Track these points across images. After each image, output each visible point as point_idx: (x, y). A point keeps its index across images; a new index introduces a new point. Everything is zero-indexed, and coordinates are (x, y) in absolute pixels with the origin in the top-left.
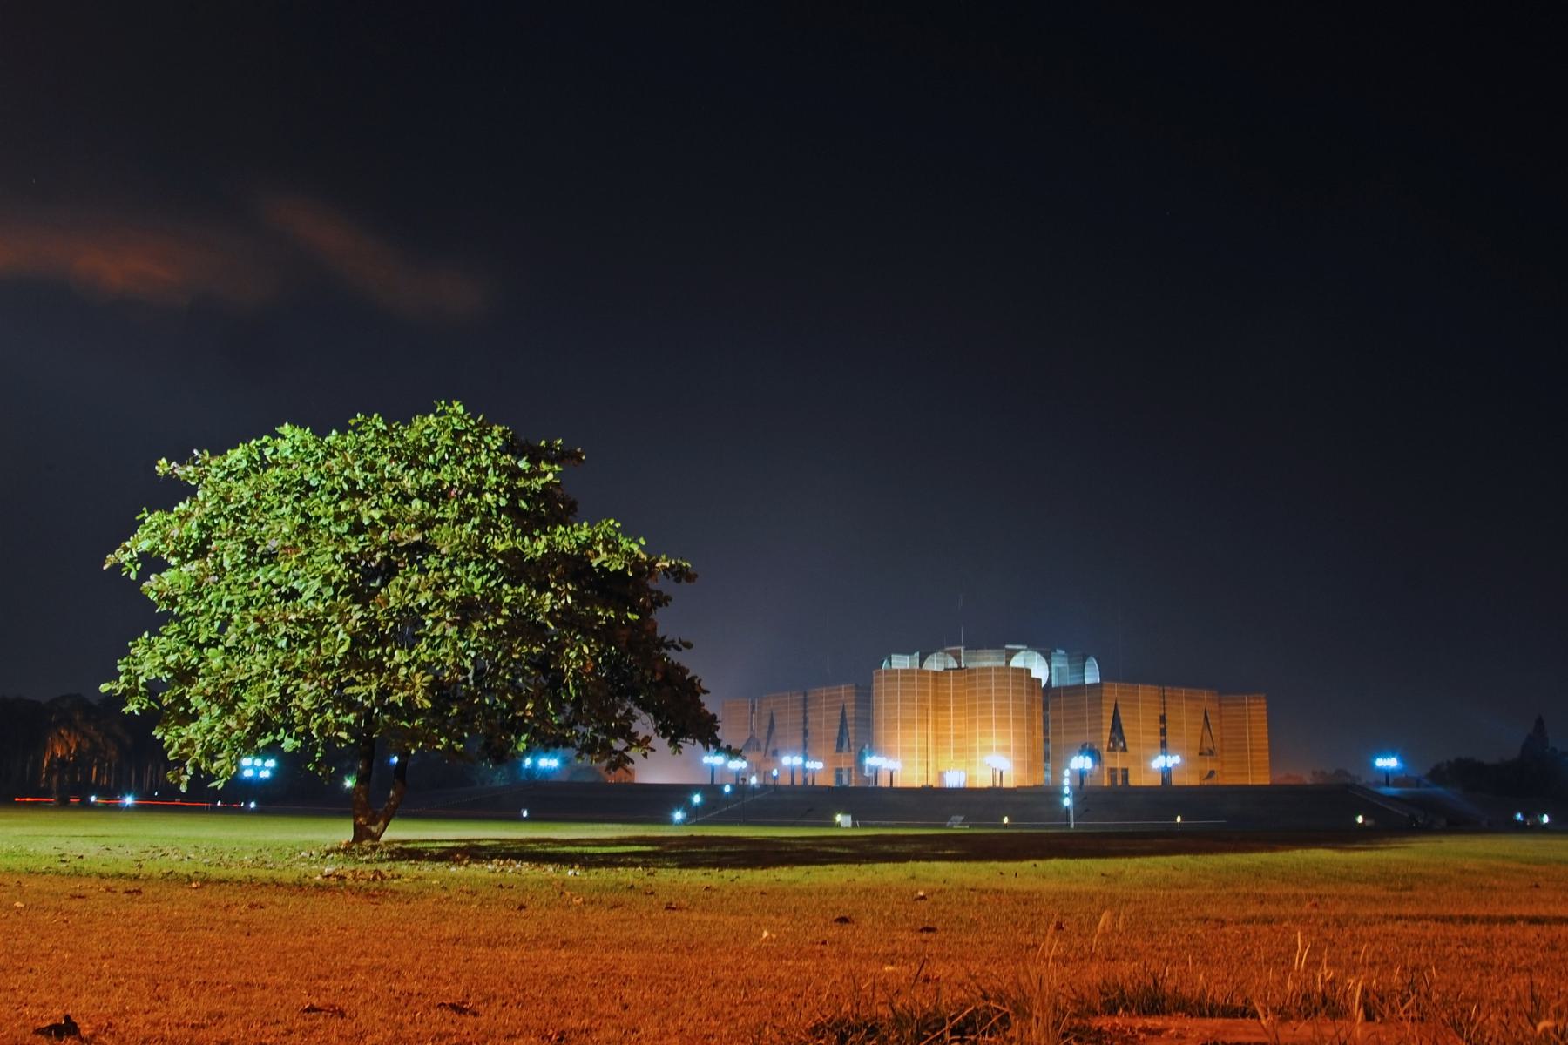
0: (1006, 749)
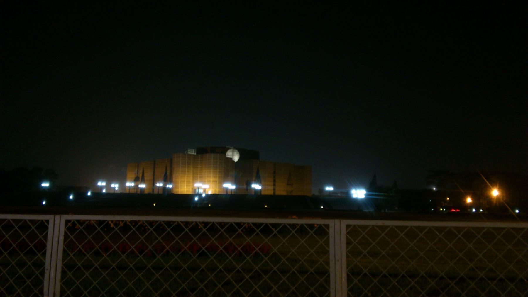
0: (216, 182)
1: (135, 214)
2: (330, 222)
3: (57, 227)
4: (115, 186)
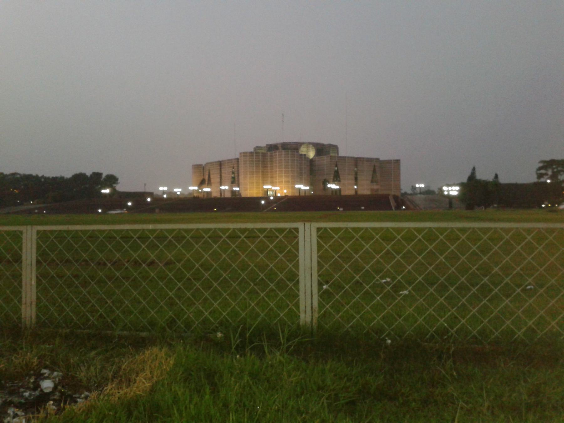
0: (288, 182)
1: (337, 221)
2: (299, 225)
3: (308, 239)
4: (178, 191)
